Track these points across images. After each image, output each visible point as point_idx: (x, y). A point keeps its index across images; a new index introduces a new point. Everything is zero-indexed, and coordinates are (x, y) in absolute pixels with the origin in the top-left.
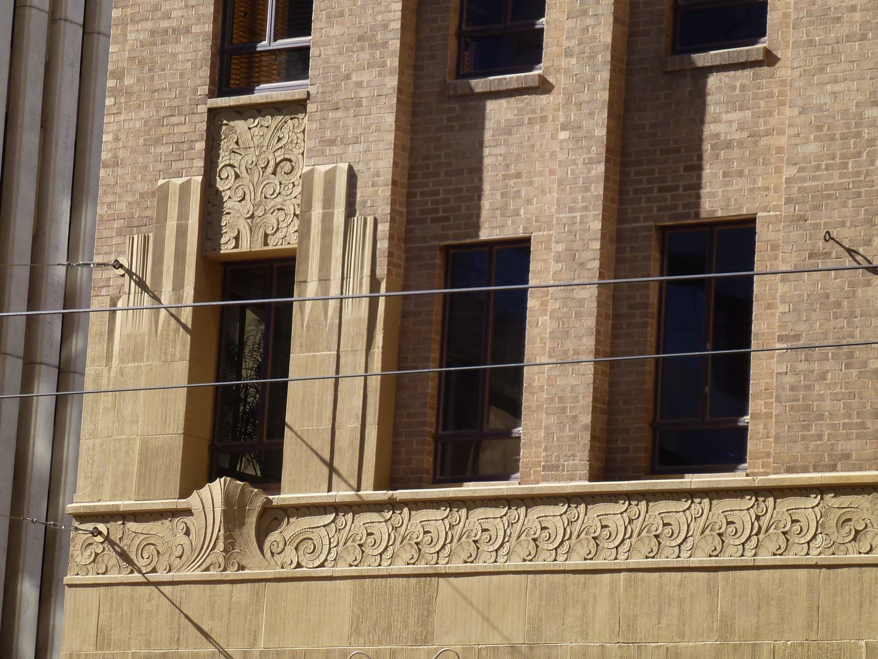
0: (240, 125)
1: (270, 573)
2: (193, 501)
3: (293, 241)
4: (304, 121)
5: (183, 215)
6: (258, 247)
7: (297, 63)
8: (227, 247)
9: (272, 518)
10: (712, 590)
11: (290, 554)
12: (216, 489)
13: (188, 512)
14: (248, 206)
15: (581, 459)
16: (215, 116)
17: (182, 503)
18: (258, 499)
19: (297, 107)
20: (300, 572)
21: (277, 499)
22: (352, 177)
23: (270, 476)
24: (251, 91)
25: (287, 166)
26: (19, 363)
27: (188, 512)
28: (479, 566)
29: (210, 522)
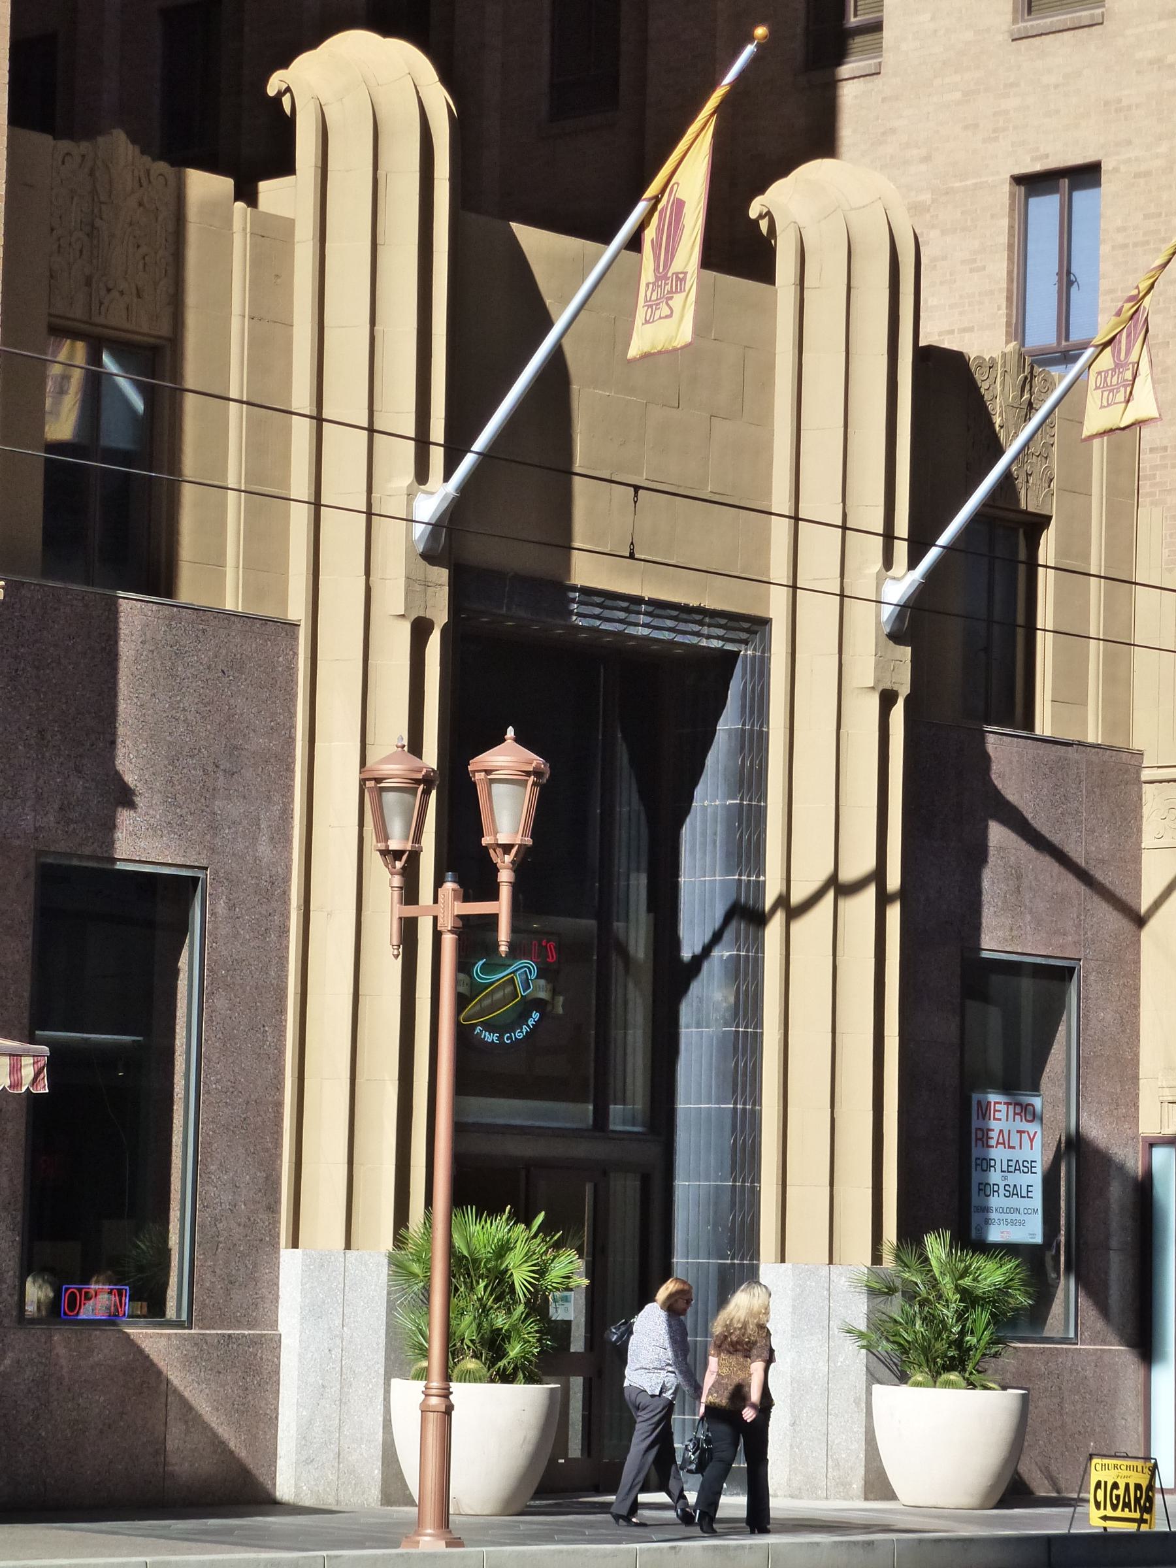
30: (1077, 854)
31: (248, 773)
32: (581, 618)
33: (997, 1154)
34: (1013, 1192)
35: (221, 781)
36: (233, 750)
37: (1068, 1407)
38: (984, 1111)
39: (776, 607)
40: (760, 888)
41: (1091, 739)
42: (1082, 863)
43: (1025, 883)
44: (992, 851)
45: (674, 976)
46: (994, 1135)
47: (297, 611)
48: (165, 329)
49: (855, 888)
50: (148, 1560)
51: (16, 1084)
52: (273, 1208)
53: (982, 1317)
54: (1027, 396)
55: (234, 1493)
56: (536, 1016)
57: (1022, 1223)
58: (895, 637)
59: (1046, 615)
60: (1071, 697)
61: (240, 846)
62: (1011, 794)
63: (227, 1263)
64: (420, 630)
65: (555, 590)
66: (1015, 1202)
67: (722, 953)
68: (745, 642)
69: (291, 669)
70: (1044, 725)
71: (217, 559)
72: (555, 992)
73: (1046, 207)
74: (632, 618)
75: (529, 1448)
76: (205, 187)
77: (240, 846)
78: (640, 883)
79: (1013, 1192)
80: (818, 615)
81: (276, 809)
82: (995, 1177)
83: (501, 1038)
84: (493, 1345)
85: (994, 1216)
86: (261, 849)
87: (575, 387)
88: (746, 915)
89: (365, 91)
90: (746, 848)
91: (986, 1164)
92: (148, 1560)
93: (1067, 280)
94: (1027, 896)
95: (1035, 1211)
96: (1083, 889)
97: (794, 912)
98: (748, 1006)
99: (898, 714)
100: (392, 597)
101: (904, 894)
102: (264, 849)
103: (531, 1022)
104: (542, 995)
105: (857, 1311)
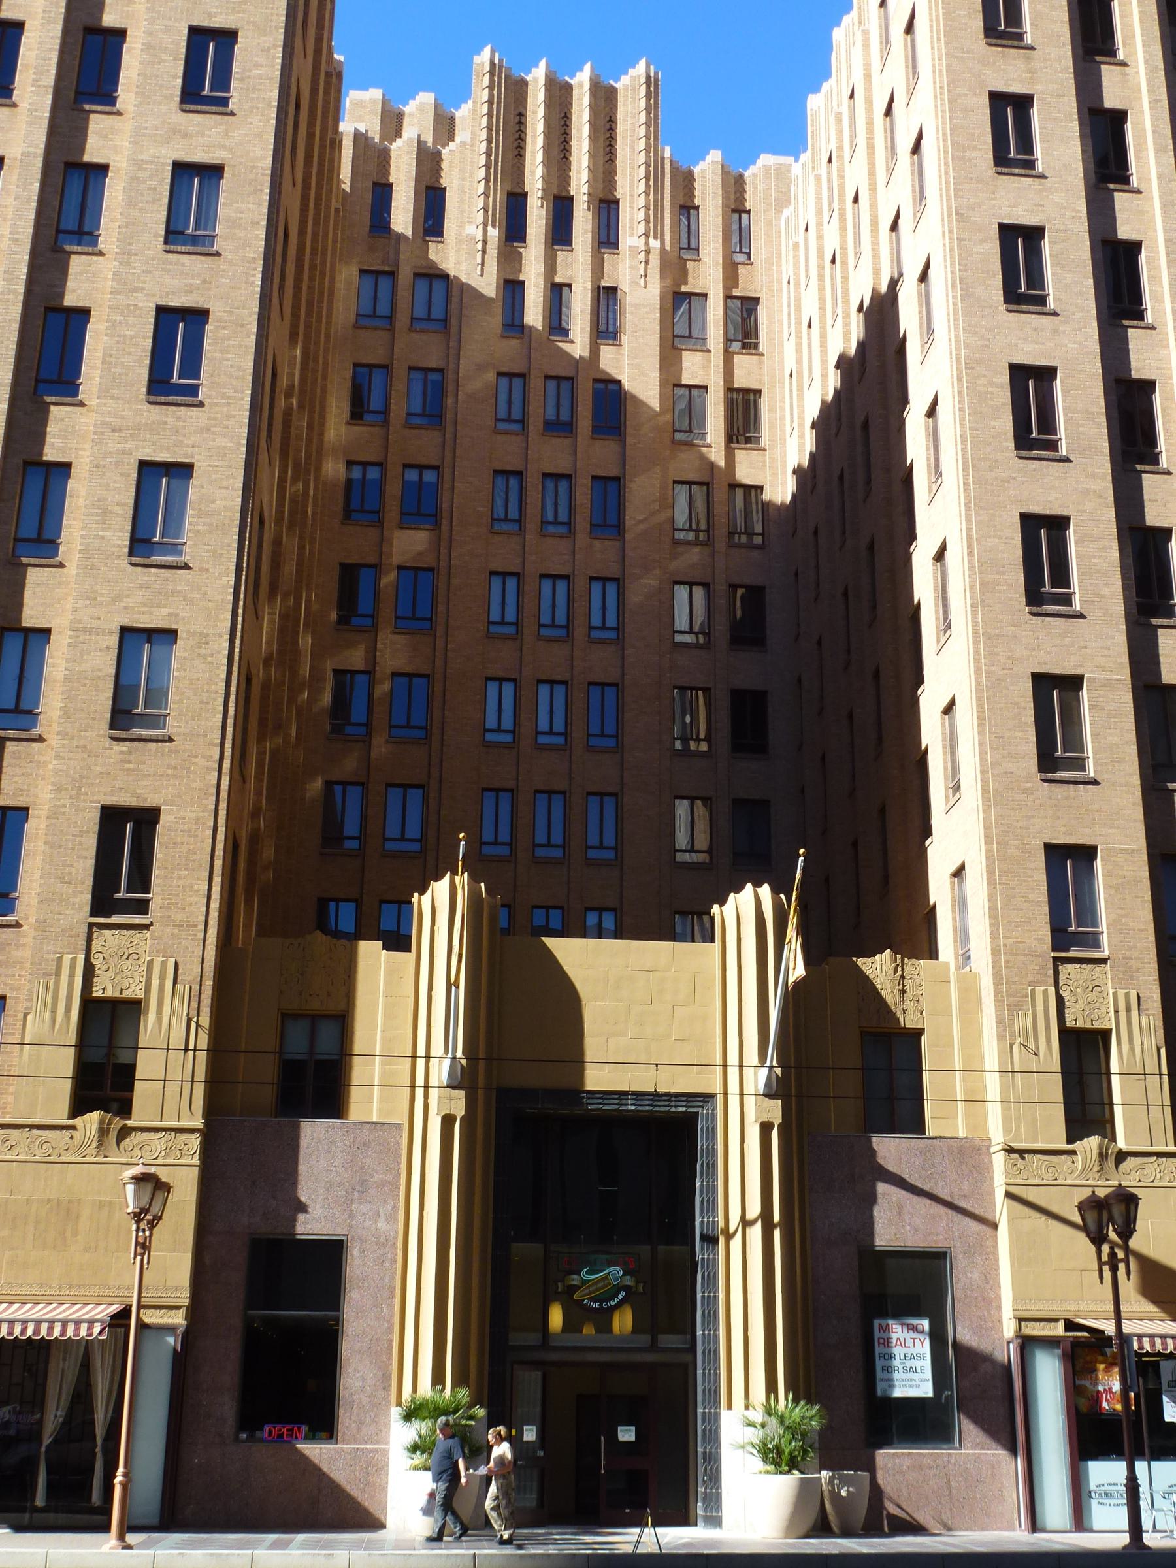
1: (124, 1160)
2: (78, 1121)
3: (140, 994)
4: (148, 934)
5: (72, 976)
6: (117, 995)
7: (142, 907)
8: (97, 992)
9: (124, 1133)
10: (1013, 1077)
11: (137, 1152)
12: (96, 1115)
13: (1074, 1152)
14: (111, 974)
15: (66, 1116)
16: (91, 925)
17: (71, 1122)
18: (118, 1123)
19: (146, 927)
20: (1140, 1184)
21: (129, 1123)
22: (176, 964)
23: (125, 1110)
24: (1067, 950)
25: (136, 957)
26: (1115, 1102)
27: (1074, 1152)
28: (182, 1161)
29: (88, 1133)
31: (373, 1192)
32: (593, 1106)
33: (897, 1351)
34: (912, 1370)
35: (356, 1196)
36: (363, 1182)
37: (953, 1484)
41: (961, 1135)
42: (949, 1199)
43: (905, 1210)
44: (879, 1196)
46: (894, 1341)
48: (342, 1007)
50: (477, 1552)
51: (91, 1335)
52: (387, 1389)
54: (899, 973)
55: (372, 1523)
56: (623, 1293)
57: (917, 1386)
61: (367, 1223)
62: (891, 1167)
63: (358, 1415)
64: (766, 1128)
65: (575, 1093)
66: (912, 1375)
68: (702, 1107)
72: (637, 1282)
74: (624, 1102)
76: (370, 952)
77: (367, 1223)
79: (912, 1370)
81: (389, 1207)
83: (601, 1305)
85: (896, 1383)
86: (379, 1225)
92: (477, 1552)
94: (907, 1218)
95: (926, 1380)
96: (949, 1211)
97: (729, 1237)
103: (620, 1297)
104: (629, 1283)
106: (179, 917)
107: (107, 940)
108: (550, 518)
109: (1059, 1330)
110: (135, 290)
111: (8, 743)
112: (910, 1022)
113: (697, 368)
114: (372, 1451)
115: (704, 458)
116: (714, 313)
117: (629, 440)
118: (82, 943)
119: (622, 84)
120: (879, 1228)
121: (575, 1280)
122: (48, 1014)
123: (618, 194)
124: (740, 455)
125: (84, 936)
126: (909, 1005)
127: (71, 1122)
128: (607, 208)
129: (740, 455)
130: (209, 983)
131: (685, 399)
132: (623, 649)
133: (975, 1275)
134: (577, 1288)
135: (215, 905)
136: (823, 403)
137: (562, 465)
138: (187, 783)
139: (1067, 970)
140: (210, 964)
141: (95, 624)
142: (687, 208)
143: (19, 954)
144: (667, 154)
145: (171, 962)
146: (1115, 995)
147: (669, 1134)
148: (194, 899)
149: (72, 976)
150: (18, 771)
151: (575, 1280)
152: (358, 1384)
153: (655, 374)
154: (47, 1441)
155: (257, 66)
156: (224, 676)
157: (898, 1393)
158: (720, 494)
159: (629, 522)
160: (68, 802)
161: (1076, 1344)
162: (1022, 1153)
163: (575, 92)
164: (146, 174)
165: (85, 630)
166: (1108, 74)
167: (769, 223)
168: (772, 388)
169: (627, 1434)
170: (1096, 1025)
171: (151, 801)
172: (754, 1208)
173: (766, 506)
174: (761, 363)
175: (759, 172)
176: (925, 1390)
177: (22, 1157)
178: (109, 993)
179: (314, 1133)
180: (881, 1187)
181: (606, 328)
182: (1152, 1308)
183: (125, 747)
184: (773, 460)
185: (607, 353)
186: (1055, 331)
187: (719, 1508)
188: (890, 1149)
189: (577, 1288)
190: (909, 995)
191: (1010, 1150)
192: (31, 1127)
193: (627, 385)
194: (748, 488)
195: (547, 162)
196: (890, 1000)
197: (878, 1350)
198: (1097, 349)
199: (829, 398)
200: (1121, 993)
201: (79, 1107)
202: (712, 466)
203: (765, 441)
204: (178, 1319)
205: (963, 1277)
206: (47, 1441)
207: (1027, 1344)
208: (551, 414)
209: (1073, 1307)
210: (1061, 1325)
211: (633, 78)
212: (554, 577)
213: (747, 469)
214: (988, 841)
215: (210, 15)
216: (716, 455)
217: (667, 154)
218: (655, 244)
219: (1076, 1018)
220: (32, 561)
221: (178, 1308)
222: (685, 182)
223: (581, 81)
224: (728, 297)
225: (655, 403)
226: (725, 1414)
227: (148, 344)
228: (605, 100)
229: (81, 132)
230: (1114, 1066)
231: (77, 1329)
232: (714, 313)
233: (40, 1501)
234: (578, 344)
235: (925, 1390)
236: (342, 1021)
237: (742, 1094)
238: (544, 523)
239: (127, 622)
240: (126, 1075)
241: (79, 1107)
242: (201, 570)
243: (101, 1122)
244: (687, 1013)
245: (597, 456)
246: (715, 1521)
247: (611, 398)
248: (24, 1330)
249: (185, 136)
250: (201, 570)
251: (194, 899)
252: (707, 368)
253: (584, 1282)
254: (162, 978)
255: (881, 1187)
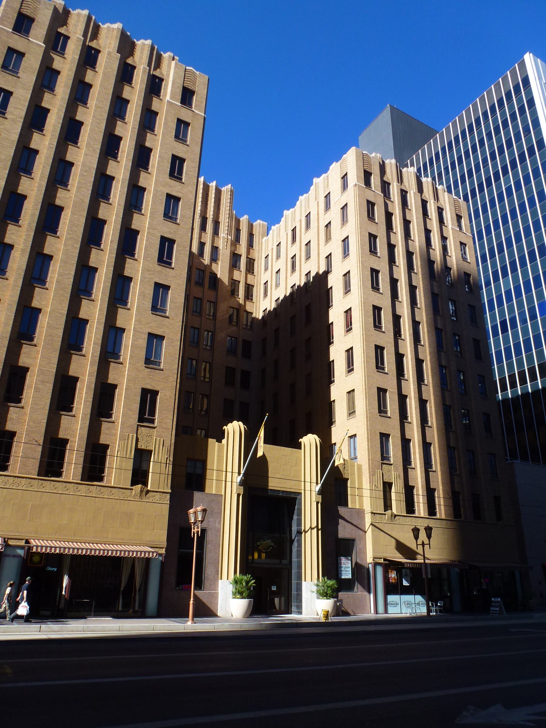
0: (143, 428)
2: (134, 487)
5: (132, 441)
8: (139, 447)
9: (148, 492)
12: (139, 486)
13: (132, 489)
15: (36, 473)
17: (131, 487)
30: (355, 523)
34: (346, 571)
38: (340, 560)
39: (303, 492)
40: (301, 529)
45: (292, 541)
47: (223, 493)
49: (314, 528)
52: (218, 574)
53: (329, 589)
58: (318, 494)
59: (349, 493)
60: (354, 502)
64: (318, 503)
67: (296, 538)
69: (222, 501)
70: (350, 506)
71: (211, 487)
73: (352, 440)
75: (246, 608)
76: (212, 442)
78: (288, 529)
79: (346, 571)
80: (308, 493)
82: (343, 569)
84: (241, 593)
87: (269, 463)
88: (299, 533)
89: (235, 429)
90: (299, 524)
91: (341, 567)
93: (355, 449)
97: (306, 532)
98: (300, 545)
99: (319, 505)
100: (314, 499)
101: (322, 529)
102: (217, 525)
105: (315, 588)
106: (164, 426)
107: (142, 430)
108: (195, 310)
109: (382, 561)
110: (154, 229)
111: (111, 363)
112: (345, 476)
113: (240, 275)
114: (214, 593)
115: (238, 302)
116: (243, 260)
117: (219, 292)
118: (135, 431)
119: (224, 189)
120: (340, 532)
121: (259, 543)
122: (125, 452)
123: (220, 220)
124: (248, 303)
125: (136, 429)
126: (346, 472)
127: (131, 487)
128: (216, 224)
129: (248, 303)
130: (173, 447)
131: (235, 283)
132: (213, 353)
133: (361, 546)
134: (259, 546)
135: (175, 423)
136: (285, 296)
137: (200, 295)
138: (167, 385)
139: (384, 466)
140: (173, 441)
141: (141, 330)
142: (238, 231)
143: (114, 432)
144: (234, 213)
145: (162, 440)
146: (156, 439)
147: (289, 502)
148: (169, 421)
149: (132, 441)
150: (114, 372)
151: (259, 543)
152: (210, 573)
153: (227, 275)
154: (122, 589)
155: (191, 171)
156: (178, 353)
157: (343, 577)
158: (242, 313)
159: (218, 316)
160: (132, 385)
161: (386, 564)
162: (374, 514)
163: (210, 188)
164: (158, 195)
165: (138, 331)
166: (143, 175)
167: (259, 240)
168: (257, 286)
169: (274, 588)
170: (148, 448)
171: (157, 388)
172: (314, 525)
173: (254, 319)
174: (255, 278)
175: (259, 224)
176: (349, 576)
177: (116, 498)
178: (143, 447)
179: (197, 495)
180: (341, 521)
181: (214, 258)
182: (401, 556)
183: (149, 370)
184: (256, 306)
185: (214, 265)
186: (382, 299)
187: (302, 609)
188: (342, 510)
189: (259, 546)
190: (346, 469)
191: (372, 513)
192: (119, 488)
193: (219, 276)
194: (248, 312)
195: (202, 206)
196: (341, 470)
197: (339, 565)
198: (391, 305)
199: (288, 295)
200: (158, 439)
201: (133, 483)
202: (240, 305)
203: (254, 300)
204: (163, 551)
205: (358, 545)
206: (122, 589)
207: (376, 564)
208: (197, 280)
209: (385, 555)
210: (382, 559)
211: (227, 189)
212: (195, 328)
213: (249, 307)
214: (367, 430)
215: (178, 153)
216: (241, 300)
217: (234, 213)
218: (229, 237)
219: (142, 445)
220: (121, 306)
221: (163, 548)
222: (238, 222)
223: (213, 184)
224: (247, 257)
225: (227, 283)
226: (304, 583)
227: (158, 246)
228: (218, 193)
229: (138, 176)
230: (152, 460)
231: (141, 554)
232: (243, 260)
233: (120, 609)
234: (206, 259)
235: (349, 576)
236: (204, 462)
237: (226, 481)
238: (193, 311)
239: (150, 331)
240: (145, 474)
241: (133, 483)
242: (172, 319)
243: (141, 488)
244: (298, 470)
245: (209, 294)
246: (300, 613)
247: (214, 279)
248: (133, 554)
249: (170, 186)
250: (172, 319)
251: (169, 421)
252: (240, 276)
253: (261, 544)
254: (159, 445)
255: (341, 521)
